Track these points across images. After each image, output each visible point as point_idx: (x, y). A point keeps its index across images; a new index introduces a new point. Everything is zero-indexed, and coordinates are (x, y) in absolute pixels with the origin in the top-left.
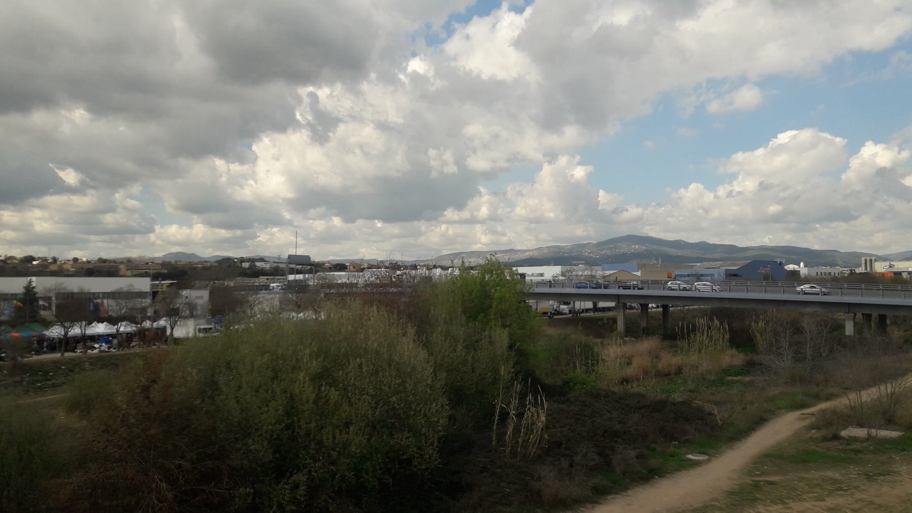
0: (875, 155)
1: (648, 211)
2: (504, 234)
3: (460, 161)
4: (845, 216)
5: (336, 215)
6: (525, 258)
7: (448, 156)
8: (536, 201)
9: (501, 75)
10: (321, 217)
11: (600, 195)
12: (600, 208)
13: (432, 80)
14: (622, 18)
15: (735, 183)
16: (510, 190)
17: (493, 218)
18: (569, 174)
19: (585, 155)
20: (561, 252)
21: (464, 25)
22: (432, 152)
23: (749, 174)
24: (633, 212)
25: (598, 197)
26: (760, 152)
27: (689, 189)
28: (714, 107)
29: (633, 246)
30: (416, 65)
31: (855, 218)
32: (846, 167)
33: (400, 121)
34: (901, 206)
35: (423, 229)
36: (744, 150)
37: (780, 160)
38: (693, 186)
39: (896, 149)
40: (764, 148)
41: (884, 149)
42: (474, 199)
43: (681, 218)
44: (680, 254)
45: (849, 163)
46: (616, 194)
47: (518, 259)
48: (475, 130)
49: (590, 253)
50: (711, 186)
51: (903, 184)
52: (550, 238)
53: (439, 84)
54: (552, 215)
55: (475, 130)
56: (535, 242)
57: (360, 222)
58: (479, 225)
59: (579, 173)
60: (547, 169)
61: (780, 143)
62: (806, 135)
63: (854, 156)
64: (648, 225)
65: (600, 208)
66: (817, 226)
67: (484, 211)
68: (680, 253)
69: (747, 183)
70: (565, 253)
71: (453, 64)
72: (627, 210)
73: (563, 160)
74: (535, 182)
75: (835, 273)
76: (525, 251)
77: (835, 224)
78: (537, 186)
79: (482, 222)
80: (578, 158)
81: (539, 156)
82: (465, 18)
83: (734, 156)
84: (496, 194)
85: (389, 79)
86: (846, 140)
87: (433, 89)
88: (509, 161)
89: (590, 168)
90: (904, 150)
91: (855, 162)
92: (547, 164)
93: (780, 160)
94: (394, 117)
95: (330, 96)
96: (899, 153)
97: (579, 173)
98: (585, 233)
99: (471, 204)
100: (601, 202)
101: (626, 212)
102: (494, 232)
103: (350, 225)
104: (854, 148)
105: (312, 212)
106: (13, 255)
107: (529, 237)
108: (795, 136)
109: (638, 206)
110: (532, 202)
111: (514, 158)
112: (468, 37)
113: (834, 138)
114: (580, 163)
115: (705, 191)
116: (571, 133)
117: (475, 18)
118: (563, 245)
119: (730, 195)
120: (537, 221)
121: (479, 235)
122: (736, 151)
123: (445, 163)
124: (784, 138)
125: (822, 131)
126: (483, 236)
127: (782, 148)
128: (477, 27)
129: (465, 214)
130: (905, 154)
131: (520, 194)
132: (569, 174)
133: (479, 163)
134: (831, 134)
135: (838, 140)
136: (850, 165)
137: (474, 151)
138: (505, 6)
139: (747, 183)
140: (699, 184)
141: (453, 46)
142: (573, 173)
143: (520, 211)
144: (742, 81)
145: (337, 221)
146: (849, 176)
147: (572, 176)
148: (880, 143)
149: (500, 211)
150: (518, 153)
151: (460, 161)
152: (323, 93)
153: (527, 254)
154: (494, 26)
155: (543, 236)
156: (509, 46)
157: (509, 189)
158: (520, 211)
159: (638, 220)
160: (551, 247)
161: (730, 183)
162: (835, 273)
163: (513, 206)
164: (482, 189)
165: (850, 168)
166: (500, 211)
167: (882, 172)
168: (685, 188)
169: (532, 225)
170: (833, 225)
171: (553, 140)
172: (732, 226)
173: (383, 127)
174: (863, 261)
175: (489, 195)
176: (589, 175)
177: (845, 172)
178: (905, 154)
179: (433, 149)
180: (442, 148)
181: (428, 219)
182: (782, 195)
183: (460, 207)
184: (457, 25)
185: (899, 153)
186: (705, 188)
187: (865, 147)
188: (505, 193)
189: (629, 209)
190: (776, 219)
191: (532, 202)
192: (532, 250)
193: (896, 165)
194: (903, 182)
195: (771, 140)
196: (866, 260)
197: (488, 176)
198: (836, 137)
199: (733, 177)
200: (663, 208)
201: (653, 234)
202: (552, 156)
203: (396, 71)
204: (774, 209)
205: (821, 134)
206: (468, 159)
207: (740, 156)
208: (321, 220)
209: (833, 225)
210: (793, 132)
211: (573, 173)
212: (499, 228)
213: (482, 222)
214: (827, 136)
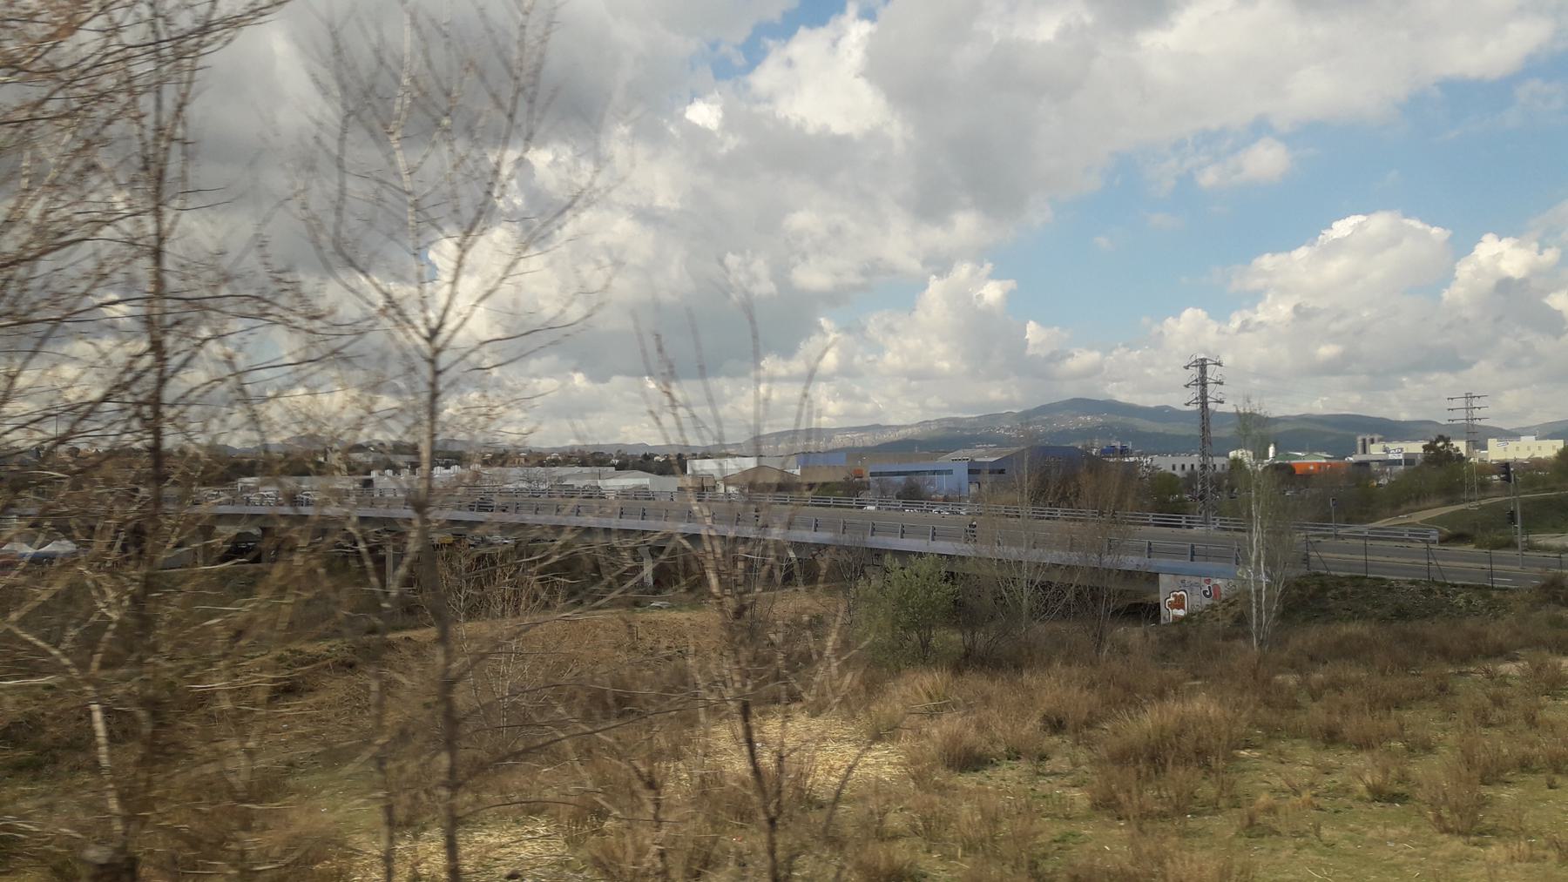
0: (1498, 257)
1: (1111, 358)
2: (865, 399)
3: (780, 274)
4: (1452, 362)
5: (576, 370)
6: (901, 438)
7: (760, 266)
8: (919, 341)
9: (839, 126)
10: (551, 373)
11: (1028, 329)
12: (1030, 352)
13: (718, 135)
14: (1046, 29)
15: (1260, 307)
16: (873, 325)
17: (846, 371)
18: (974, 295)
19: (1000, 262)
20: (958, 429)
21: (783, 42)
22: (732, 260)
23: (1283, 291)
24: (1083, 359)
25: (1025, 333)
26: (1302, 253)
27: (1182, 319)
28: (1209, 177)
29: (1082, 418)
30: (704, 114)
31: (1468, 365)
32: (1448, 278)
33: (676, 205)
34: (1544, 344)
35: (727, 391)
36: (1274, 250)
37: (1336, 268)
38: (1188, 313)
39: (1535, 245)
40: (1309, 246)
41: (1513, 246)
42: (811, 339)
43: (1169, 369)
44: (1161, 431)
45: (1455, 271)
46: (1056, 329)
47: (886, 441)
48: (802, 220)
49: (1008, 430)
50: (1220, 313)
51: (1548, 306)
52: (945, 405)
53: (732, 142)
54: (946, 365)
55: (802, 220)
56: (919, 412)
57: (617, 381)
58: (824, 384)
59: (992, 292)
60: (935, 287)
61: (1335, 237)
62: (1379, 223)
63: (1462, 260)
64: (1113, 381)
65: (1030, 352)
66: (1404, 379)
67: (831, 360)
68: (1160, 428)
69: (1280, 307)
70: (965, 430)
71: (763, 108)
72: (1072, 355)
73: (963, 271)
74: (914, 310)
75: (1192, 466)
76: (898, 428)
77: (1435, 376)
78: (920, 315)
79: (828, 378)
80: (988, 266)
81: (915, 265)
82: (785, 29)
83: (1257, 261)
84: (847, 330)
85: (651, 134)
86: (1449, 232)
87: (724, 151)
88: (864, 273)
89: (1010, 284)
90: (1550, 247)
91: (1464, 270)
92: (934, 277)
93: (1336, 268)
94: (665, 198)
95: (555, 163)
96: (1540, 253)
97: (992, 292)
98: (1005, 396)
99: (809, 347)
100: (1031, 342)
101: (1069, 360)
102: (848, 395)
103: (601, 386)
104: (1463, 246)
105: (534, 364)
106: (1163, 404)
107: (910, 404)
108: (1360, 224)
109: (1091, 348)
110: (912, 343)
111: (873, 269)
112: (790, 63)
113: (1428, 227)
114: (993, 276)
115: (1210, 321)
116: (966, 224)
117: (802, 31)
118: (965, 416)
119: (1244, 327)
120: (921, 376)
121: (823, 400)
122: (1261, 253)
123: (754, 279)
124: (1342, 228)
125: (1407, 216)
126: (831, 403)
127: (1339, 245)
128: (806, 46)
129: (798, 366)
130: (1551, 255)
131: (890, 329)
132: (974, 295)
133: (812, 277)
134: (1422, 220)
135: (1435, 231)
136: (1457, 274)
137: (804, 257)
138: (852, 10)
139: (1280, 307)
140: (1200, 311)
141: (765, 77)
142: (982, 292)
143: (892, 359)
144: (1260, 129)
145: (579, 379)
146: (1456, 293)
147: (980, 297)
148: (1508, 236)
149: (857, 360)
150: (880, 259)
151: (780, 274)
152: (541, 158)
153: (902, 432)
154: (834, 43)
155: (933, 402)
156: (857, 77)
157: (872, 321)
158: (892, 359)
159: (1094, 371)
160: (943, 420)
161: (1252, 306)
162: (1192, 466)
163: (880, 350)
164: (823, 321)
165: (1456, 279)
166: (857, 360)
167: (1505, 286)
168: (1174, 317)
169: (914, 383)
170: (1432, 378)
171: (934, 236)
172: (1257, 382)
173: (646, 216)
174: (1360, 443)
175: (837, 332)
176: (1010, 297)
177: (1448, 287)
178: (1551, 255)
179: (734, 253)
180: (748, 252)
181: (732, 375)
182: (1335, 327)
183: (788, 352)
184: (770, 43)
185: (1540, 253)
186: (1210, 316)
187: (1481, 244)
188: (863, 329)
189: (1076, 354)
190: (1331, 368)
191: (912, 343)
192: (911, 426)
193: (1535, 272)
194: (1547, 301)
195: (1320, 233)
196: (1364, 440)
197: (833, 298)
198: (1432, 227)
199: (1256, 297)
200: (1138, 352)
201: (1122, 398)
202: (941, 264)
203: (665, 121)
204: (1327, 351)
205: (1408, 222)
206: (794, 271)
207: (1267, 261)
208: (551, 377)
209: (1432, 378)
210: (1360, 218)
211: (982, 292)
212: (858, 389)
213: (828, 378)
214: (1416, 224)
